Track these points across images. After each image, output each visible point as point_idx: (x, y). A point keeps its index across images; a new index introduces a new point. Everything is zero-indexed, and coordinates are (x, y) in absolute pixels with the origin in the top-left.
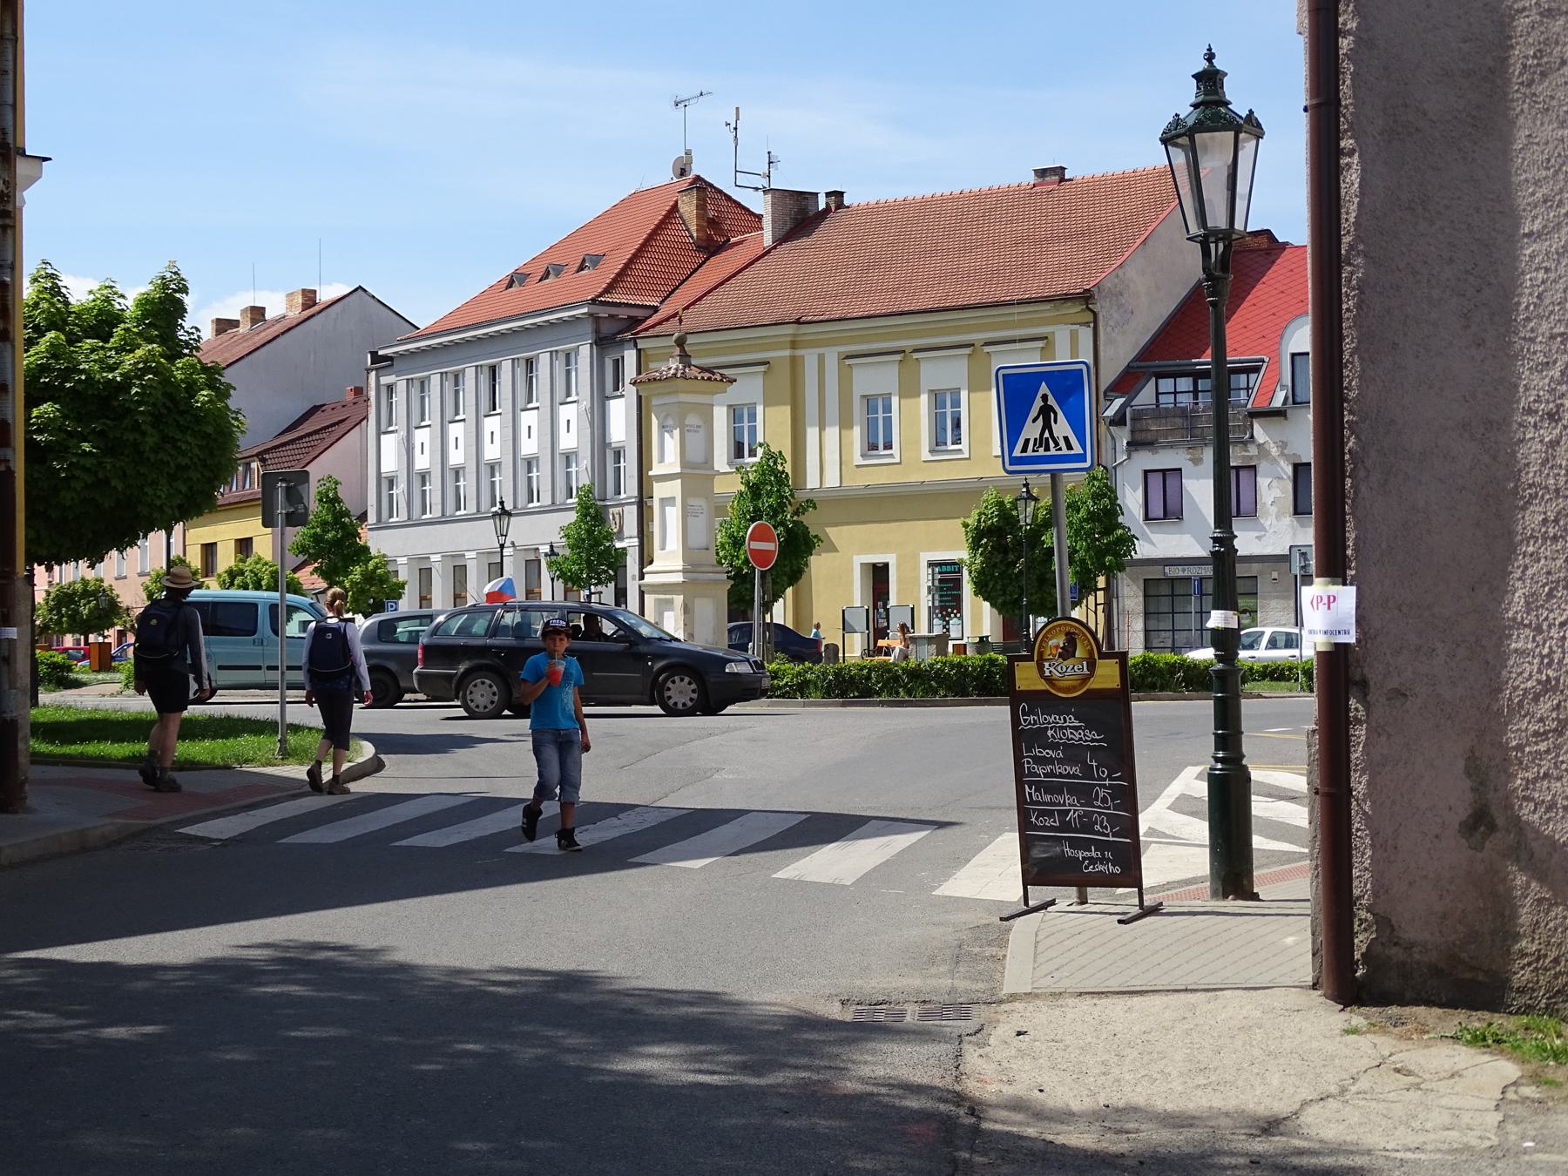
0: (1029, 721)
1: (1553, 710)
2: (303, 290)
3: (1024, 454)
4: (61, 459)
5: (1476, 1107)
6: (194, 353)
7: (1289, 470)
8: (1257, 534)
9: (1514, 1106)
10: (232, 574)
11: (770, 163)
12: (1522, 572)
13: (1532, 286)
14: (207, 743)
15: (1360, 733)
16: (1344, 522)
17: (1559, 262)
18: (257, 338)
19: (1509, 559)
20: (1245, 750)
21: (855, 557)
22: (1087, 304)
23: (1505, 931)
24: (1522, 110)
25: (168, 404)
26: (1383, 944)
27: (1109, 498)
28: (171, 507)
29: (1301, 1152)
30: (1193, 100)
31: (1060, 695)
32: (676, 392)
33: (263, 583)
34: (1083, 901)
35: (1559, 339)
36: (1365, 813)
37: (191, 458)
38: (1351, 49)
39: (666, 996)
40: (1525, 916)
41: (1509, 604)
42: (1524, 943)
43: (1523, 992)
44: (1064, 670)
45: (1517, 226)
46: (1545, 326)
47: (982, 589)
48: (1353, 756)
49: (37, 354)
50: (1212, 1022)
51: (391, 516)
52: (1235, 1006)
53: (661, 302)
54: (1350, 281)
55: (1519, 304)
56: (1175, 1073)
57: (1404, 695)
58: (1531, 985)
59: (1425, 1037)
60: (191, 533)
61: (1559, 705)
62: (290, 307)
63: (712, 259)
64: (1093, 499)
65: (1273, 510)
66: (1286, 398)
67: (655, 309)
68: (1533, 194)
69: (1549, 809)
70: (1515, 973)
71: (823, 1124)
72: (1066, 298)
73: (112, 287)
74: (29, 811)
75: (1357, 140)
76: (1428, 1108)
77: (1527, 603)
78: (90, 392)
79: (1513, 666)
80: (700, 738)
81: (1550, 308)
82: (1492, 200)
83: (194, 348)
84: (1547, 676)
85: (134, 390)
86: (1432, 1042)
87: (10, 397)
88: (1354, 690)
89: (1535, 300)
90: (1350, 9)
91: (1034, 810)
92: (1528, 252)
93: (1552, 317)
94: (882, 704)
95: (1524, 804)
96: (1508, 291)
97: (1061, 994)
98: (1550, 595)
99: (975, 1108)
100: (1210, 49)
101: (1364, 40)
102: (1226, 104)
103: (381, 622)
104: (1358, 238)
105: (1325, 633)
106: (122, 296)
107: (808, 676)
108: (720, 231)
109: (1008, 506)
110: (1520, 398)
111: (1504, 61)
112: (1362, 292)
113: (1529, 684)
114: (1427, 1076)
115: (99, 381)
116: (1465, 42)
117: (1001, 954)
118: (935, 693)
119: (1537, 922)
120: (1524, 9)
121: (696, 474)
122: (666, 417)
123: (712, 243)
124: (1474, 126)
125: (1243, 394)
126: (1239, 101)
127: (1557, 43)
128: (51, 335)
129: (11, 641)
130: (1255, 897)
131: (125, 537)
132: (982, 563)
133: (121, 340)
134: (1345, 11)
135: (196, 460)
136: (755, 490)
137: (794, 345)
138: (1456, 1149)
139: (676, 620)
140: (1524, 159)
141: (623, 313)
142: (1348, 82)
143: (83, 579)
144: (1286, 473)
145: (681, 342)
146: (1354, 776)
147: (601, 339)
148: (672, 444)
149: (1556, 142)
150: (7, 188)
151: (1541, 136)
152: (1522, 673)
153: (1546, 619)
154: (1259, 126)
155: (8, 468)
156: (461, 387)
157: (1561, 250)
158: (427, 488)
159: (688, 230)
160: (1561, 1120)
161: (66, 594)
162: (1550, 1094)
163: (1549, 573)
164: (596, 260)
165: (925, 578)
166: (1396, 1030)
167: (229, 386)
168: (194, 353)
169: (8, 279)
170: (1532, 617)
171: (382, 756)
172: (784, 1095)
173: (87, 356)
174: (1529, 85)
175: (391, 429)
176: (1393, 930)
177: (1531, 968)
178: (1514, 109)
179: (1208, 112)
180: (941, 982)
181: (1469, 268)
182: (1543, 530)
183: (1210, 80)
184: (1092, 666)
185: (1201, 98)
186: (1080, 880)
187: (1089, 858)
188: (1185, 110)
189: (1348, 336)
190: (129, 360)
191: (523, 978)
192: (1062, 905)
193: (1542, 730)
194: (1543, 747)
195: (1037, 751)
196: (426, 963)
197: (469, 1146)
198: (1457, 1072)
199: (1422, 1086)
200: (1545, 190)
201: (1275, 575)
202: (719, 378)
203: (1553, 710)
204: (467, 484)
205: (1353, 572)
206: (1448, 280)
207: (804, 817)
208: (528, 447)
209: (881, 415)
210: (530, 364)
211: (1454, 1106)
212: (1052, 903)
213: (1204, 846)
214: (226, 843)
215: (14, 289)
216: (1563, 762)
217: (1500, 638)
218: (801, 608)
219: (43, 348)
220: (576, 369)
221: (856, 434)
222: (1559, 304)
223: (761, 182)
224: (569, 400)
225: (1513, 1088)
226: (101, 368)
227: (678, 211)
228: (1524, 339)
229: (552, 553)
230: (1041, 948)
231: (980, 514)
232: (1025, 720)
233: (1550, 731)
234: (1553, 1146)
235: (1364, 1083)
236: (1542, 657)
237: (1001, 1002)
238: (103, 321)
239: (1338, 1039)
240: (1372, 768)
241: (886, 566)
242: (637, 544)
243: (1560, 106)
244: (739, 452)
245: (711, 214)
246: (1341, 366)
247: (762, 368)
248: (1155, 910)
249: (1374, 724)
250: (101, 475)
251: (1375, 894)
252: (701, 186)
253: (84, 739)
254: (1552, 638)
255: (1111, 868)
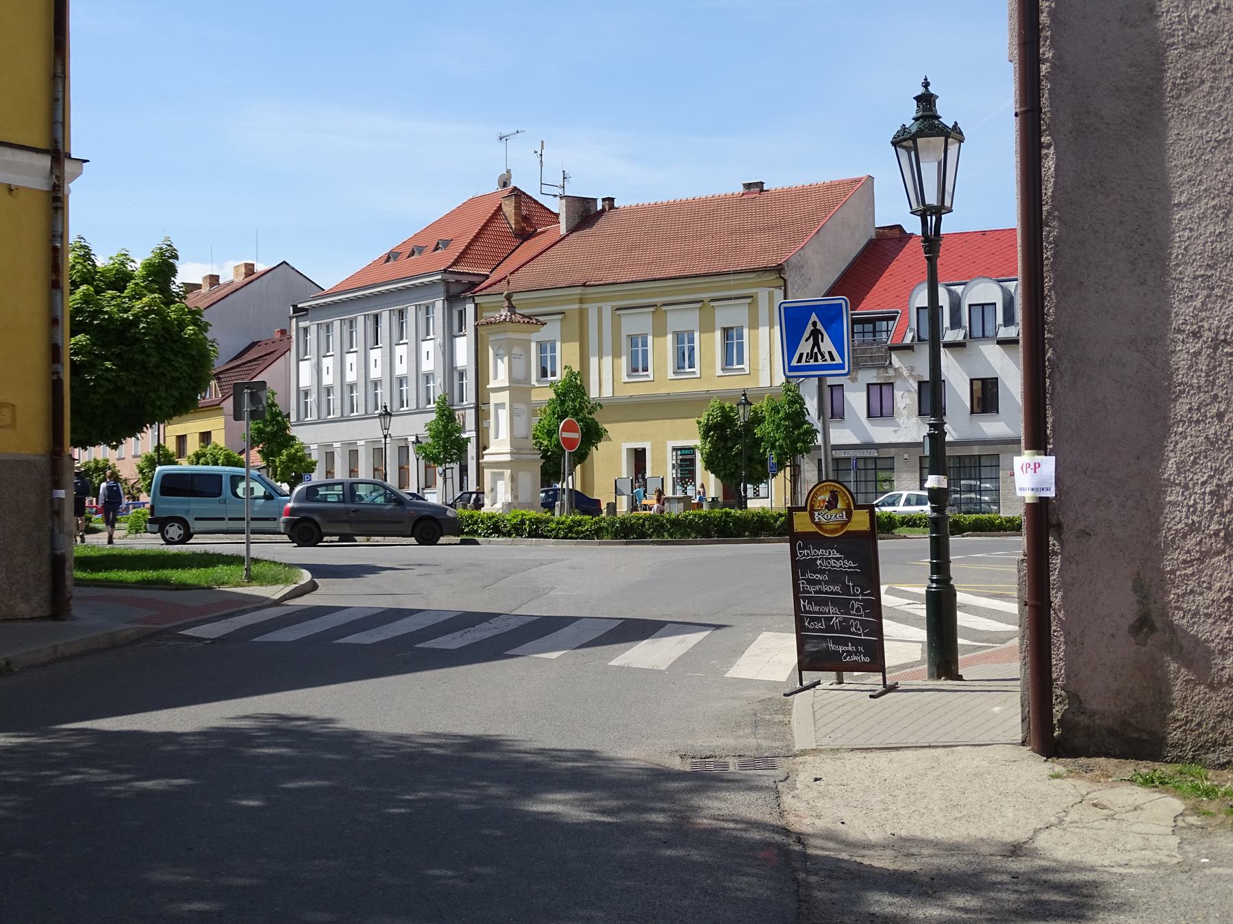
0: (803, 554)
1: (1197, 544)
2: (246, 264)
3: (799, 364)
4: (91, 373)
5: (1158, 832)
6: (183, 301)
7: (916, 386)
8: (895, 428)
9: (1184, 831)
10: (198, 456)
11: (564, 178)
12: (1174, 446)
13: (1180, 241)
14: (194, 571)
15: (1056, 562)
16: (1045, 410)
17: (1200, 225)
18: (214, 296)
19: (1165, 436)
20: (952, 574)
21: (623, 444)
22: (780, 274)
23: (1163, 703)
24: (1173, 116)
25: (166, 335)
26: (1073, 713)
27: (800, 404)
28: (168, 407)
29: (1046, 870)
30: (914, 115)
31: (826, 535)
32: (506, 332)
33: (219, 462)
34: (840, 682)
35: (1200, 279)
36: (1060, 619)
37: (181, 373)
38: (1048, 72)
39: (555, 753)
40: (1177, 693)
41: (1165, 469)
42: (1176, 712)
43: (1175, 747)
44: (829, 516)
45: (1170, 198)
46: (1190, 270)
47: (710, 465)
48: (1052, 578)
49: (74, 300)
50: (955, 771)
51: (306, 416)
52: (968, 759)
53: (491, 272)
54: (1048, 238)
55: (1171, 254)
56: (936, 809)
57: (1090, 534)
58: (1181, 742)
59: (1110, 780)
60: (169, 428)
61: (1201, 541)
62: (237, 275)
63: (525, 243)
64: (788, 404)
65: (905, 412)
66: (913, 337)
67: (487, 277)
68: (1181, 176)
69: (1194, 616)
70: (1170, 733)
71: (696, 855)
72: (765, 270)
73: (126, 255)
74: (74, 619)
75: (1052, 137)
76: (1125, 834)
77: (1178, 468)
78: (111, 327)
79: (1167, 514)
80: (536, 566)
81: (1194, 257)
82: (1151, 180)
83: (182, 297)
84: (1192, 520)
85: (142, 326)
86: (1115, 784)
87: (60, 328)
88: (1052, 530)
89: (1182, 251)
90: (1048, 43)
91: (807, 617)
92: (1177, 217)
93: (1195, 263)
94: (653, 543)
95: (1176, 612)
96: (1164, 244)
97: (838, 749)
98: (1194, 463)
99: (800, 838)
100: (926, 79)
101: (1058, 66)
102: (938, 118)
103: (308, 488)
104: (1054, 207)
105: (1032, 490)
106: (133, 261)
107: (602, 524)
108: (530, 224)
109: (728, 409)
110: (1172, 322)
111: (1159, 81)
112: (1057, 246)
113: (1179, 526)
114: (1117, 809)
115: (117, 319)
116: (1131, 66)
117: (786, 720)
118: (689, 536)
119: (1186, 697)
120: (1174, 44)
121: (519, 388)
122: (500, 347)
123: (525, 233)
124: (1137, 127)
125: (884, 335)
126: (947, 114)
127: (1198, 68)
128: (84, 287)
129: (61, 500)
130: (960, 678)
131: (134, 429)
132: (710, 448)
133: (133, 291)
134: (1044, 45)
135: (184, 375)
136: (562, 396)
137: (581, 301)
138: (1154, 865)
139: (506, 487)
140: (1174, 151)
141: (465, 279)
142: (1046, 96)
143: (95, 459)
144: (913, 388)
145: (508, 297)
146: (1053, 592)
147: (450, 297)
148: (503, 367)
149: (1197, 139)
150: (58, 181)
151: (1186, 135)
152: (1174, 518)
153: (1192, 479)
154: (961, 133)
155: (59, 377)
156: (354, 329)
157: (1201, 216)
158: (331, 397)
159: (509, 223)
160: (1222, 841)
162: (1208, 822)
163: (1193, 447)
164: (446, 243)
165: (670, 459)
166: (1088, 775)
167: (207, 324)
168: (183, 301)
169: (59, 245)
170: (1181, 478)
171: (315, 580)
172: (660, 829)
173: (108, 302)
174: (1177, 98)
175: (306, 357)
176: (1081, 703)
177: (1181, 730)
178: (1167, 115)
179: (925, 123)
180: (750, 742)
181: (1134, 228)
182: (1189, 416)
183: (926, 100)
184: (849, 514)
185: (920, 114)
186: (837, 665)
187: (846, 652)
188: (909, 122)
189: (1047, 277)
190: (138, 305)
191: (448, 741)
192: (825, 684)
193: (1189, 559)
194: (1189, 571)
195: (809, 575)
196: (376, 730)
197: (437, 872)
198: (1138, 806)
199: (1115, 816)
200: (1189, 173)
201: (906, 456)
202: (534, 321)
203: (1197, 544)
204: (359, 395)
205: (1051, 446)
206: (1120, 237)
207: (620, 622)
208: (375, 373)
209: (640, 349)
210: (401, 313)
211: (1144, 832)
212: (818, 683)
213: (887, 640)
214: (214, 641)
215: (63, 252)
216: (1204, 582)
217: (1158, 493)
218: (587, 478)
219: (78, 296)
220: (433, 317)
221: (624, 361)
222: (1200, 254)
223: (558, 191)
224: (428, 338)
225: (1180, 818)
226: (118, 310)
227: (502, 211)
228: (1175, 279)
229: (418, 441)
230: (818, 715)
231: (709, 415)
232: (801, 554)
233: (1194, 560)
234: (1222, 861)
235: (1073, 815)
236: (1189, 507)
237: (796, 756)
238: (120, 279)
239: (1047, 782)
240: (1065, 586)
241: (644, 450)
243: (1200, 113)
244: (544, 373)
245: (524, 213)
246: (1043, 298)
247: (560, 317)
248: (893, 688)
249: (1067, 555)
250: (119, 384)
251: (1068, 677)
252: (517, 194)
253: (108, 568)
254: (1196, 493)
255: (863, 658)
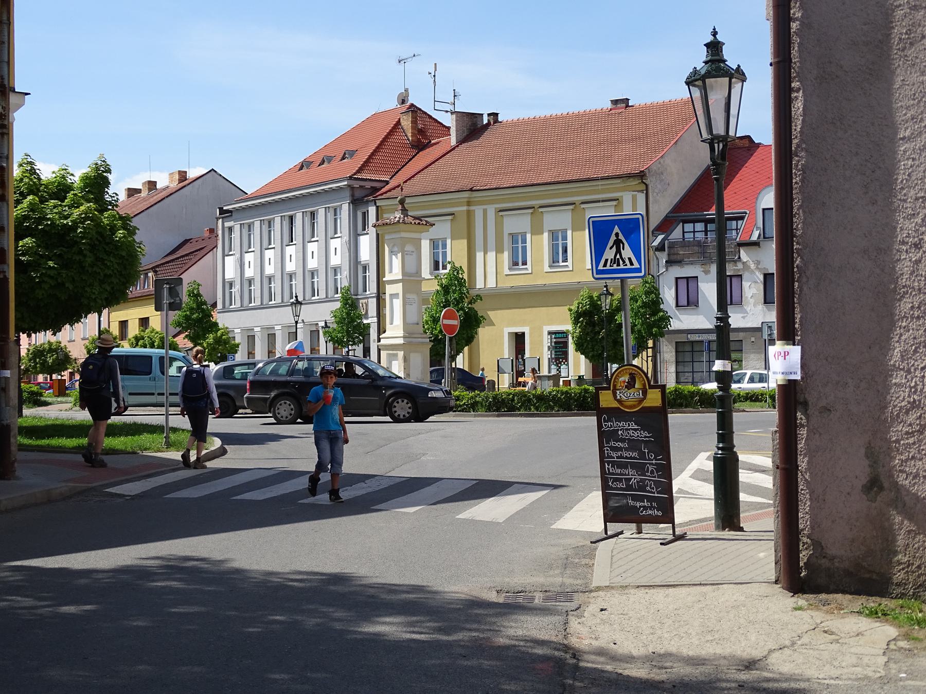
0: (608, 426)
1: (917, 419)
2: (179, 171)
3: (605, 268)
4: (36, 271)
5: (871, 653)
6: (115, 208)
7: (761, 277)
8: (742, 315)
9: (894, 653)
10: (137, 339)
11: (455, 96)
12: (899, 338)
13: (905, 169)
14: (122, 438)
15: (803, 433)
16: (794, 308)
17: (921, 155)
18: (152, 200)
19: (891, 330)
20: (735, 442)
21: (505, 329)
22: (642, 179)
23: (889, 549)
24: (899, 65)
25: (100, 238)
26: (817, 557)
27: (655, 294)
28: (101, 299)
29: (768, 680)
30: (704, 59)
31: (626, 410)
32: (399, 232)
33: (155, 344)
34: (640, 532)
35: (921, 200)
36: (806, 480)
37: (113, 270)
38: (798, 29)
39: (394, 588)
40: (901, 541)
41: (891, 356)
42: (900, 557)
43: (899, 585)
44: (629, 395)
45: (896, 133)
46: (912, 193)
47: (580, 348)
48: (799, 446)
49: (22, 209)
50: (716, 603)
51: (231, 304)
52: (729, 594)
53: (391, 178)
54: (797, 166)
55: (897, 179)
56: (694, 633)
57: (829, 410)
58: (904, 581)
59: (842, 612)
60: (113, 315)
61: (920, 416)
62: (171, 181)
63: (421, 153)
64: (645, 294)
65: (752, 301)
66: (760, 235)
67: (387, 183)
68: (905, 114)
69: (915, 477)
70: (895, 574)
71: (486, 663)
72: (630, 176)
73: (66, 169)
74: (17, 478)
75: (801, 83)
76: (843, 654)
77: (902, 356)
78: (53, 232)
79: (893, 393)
80: (413, 435)
81: (916, 182)
82: (881, 118)
83: (115, 205)
84: (914, 399)
85: (79, 230)
86: (846, 615)
87: (6, 235)
88: (799, 407)
89: (906, 177)
90: (797, 5)
91: (611, 478)
92: (902, 149)
93: (917, 187)
94: (521, 415)
95: (900, 475)
96: (891, 172)
97: (626, 586)
98: (915, 351)
99: (576, 654)
100: (714, 29)
101: (805, 24)
102: (724, 61)
103: (225, 367)
104: (802, 141)
105: (783, 373)
106: (72, 175)
107: (477, 399)
108: (425, 137)
109: (596, 299)
110: (898, 235)
111: (888, 36)
112: (804, 172)
113: (903, 404)
114: (842, 635)
115: (58, 225)
116: (865, 25)
117: (591, 563)
118: (552, 409)
119: (908, 544)
120: (900, 5)
121: (411, 280)
122: (393, 246)
123: (420, 144)
124: (871, 74)
125: (734, 232)
126: (732, 59)
127: (919, 25)
128: (30, 197)
129: (6, 378)
130: (741, 529)
131: (74, 317)
132: (580, 332)
133: (72, 201)
134: (794, 7)
135: (115, 271)
136: (446, 289)
137: (469, 204)
138: (860, 678)
139: (399, 366)
140: (900, 94)
141: (368, 185)
142: (796, 48)
143: (49, 342)
144: (759, 279)
145: (402, 202)
146: (800, 458)
147: (355, 200)
148: (397, 262)
149: (919, 84)
150: (4, 111)
151: (910, 81)
152: (899, 397)
153: (913, 365)
154: (743, 74)
155: (5, 276)
156: (272, 229)
157: (922, 148)
158: (252, 288)
159: (406, 136)
160: (922, 661)
161: (39, 350)
162: (916, 645)
163: (915, 338)
164: (352, 153)
165: (546, 341)
166: (825, 608)
167: (135, 228)
168: (115, 208)
169: (5, 165)
170: (905, 364)
171: (226, 446)
172: (463, 646)
173: (51, 210)
174: (903, 50)
175: (231, 253)
176: (823, 549)
177: (904, 571)
178: (894, 65)
179: (713, 66)
180: (556, 580)
181: (867, 158)
182: (911, 313)
183: (714, 47)
184: (645, 393)
185: (709, 58)
186: (638, 519)
187: (643, 507)
188: (700, 65)
189: (796, 198)
190: (76, 213)
191: (309, 577)
192: (627, 534)
193: (910, 431)
194: (911, 441)
195: (612, 443)
196: (252, 569)
197: (277, 676)
198: (860, 633)
199: (840, 641)
200: (912, 112)
201: (753, 339)
202: (424, 223)
203: (917, 419)
204: (276, 286)
205: (799, 338)
206: (855, 165)
207: (475, 482)
208: (312, 264)
209: (520, 245)
210: (313, 215)
211: (859, 653)
212: (621, 533)
213: (711, 499)
214: (133, 497)
215: (8, 171)
216: (923, 450)
217: (886, 376)
218: (473, 359)
219: (25, 205)
220: (340, 218)
221: (506, 256)
222: (921, 179)
223: (449, 108)
224: (336, 236)
225: (893, 642)
226: (60, 217)
227: (400, 125)
228: (900, 200)
229: (326, 326)
230: (615, 559)
231: (579, 304)
232: (605, 425)
233: (915, 431)
234: (917, 676)
235: (805, 639)
236: (911, 388)
237: (591, 591)
238: (61, 189)
239: (790, 613)
240: (810, 453)
241: (523, 334)
242: (376, 321)
243: (921, 62)
244: (436, 267)
245: (420, 126)
246: (792, 216)
247: (450, 217)
248: (682, 537)
249: (811, 427)
250: (59, 281)
251: (812, 528)
252: (414, 110)
253: (50, 436)
254: (916, 376)
255: (656, 512)
